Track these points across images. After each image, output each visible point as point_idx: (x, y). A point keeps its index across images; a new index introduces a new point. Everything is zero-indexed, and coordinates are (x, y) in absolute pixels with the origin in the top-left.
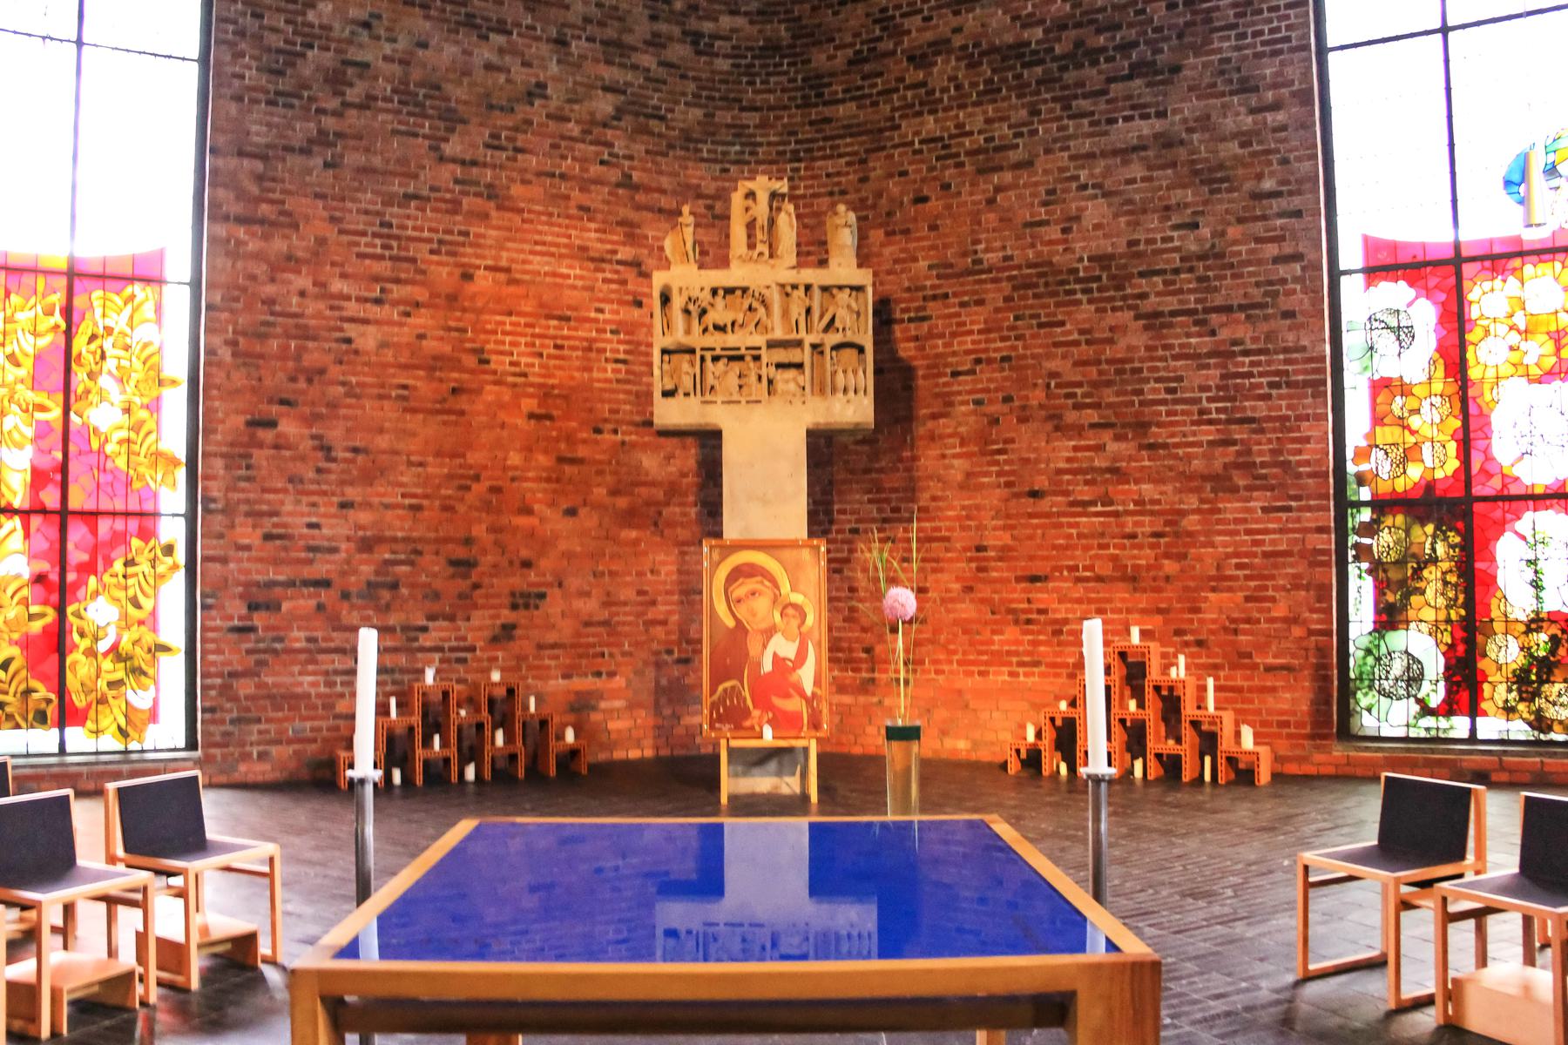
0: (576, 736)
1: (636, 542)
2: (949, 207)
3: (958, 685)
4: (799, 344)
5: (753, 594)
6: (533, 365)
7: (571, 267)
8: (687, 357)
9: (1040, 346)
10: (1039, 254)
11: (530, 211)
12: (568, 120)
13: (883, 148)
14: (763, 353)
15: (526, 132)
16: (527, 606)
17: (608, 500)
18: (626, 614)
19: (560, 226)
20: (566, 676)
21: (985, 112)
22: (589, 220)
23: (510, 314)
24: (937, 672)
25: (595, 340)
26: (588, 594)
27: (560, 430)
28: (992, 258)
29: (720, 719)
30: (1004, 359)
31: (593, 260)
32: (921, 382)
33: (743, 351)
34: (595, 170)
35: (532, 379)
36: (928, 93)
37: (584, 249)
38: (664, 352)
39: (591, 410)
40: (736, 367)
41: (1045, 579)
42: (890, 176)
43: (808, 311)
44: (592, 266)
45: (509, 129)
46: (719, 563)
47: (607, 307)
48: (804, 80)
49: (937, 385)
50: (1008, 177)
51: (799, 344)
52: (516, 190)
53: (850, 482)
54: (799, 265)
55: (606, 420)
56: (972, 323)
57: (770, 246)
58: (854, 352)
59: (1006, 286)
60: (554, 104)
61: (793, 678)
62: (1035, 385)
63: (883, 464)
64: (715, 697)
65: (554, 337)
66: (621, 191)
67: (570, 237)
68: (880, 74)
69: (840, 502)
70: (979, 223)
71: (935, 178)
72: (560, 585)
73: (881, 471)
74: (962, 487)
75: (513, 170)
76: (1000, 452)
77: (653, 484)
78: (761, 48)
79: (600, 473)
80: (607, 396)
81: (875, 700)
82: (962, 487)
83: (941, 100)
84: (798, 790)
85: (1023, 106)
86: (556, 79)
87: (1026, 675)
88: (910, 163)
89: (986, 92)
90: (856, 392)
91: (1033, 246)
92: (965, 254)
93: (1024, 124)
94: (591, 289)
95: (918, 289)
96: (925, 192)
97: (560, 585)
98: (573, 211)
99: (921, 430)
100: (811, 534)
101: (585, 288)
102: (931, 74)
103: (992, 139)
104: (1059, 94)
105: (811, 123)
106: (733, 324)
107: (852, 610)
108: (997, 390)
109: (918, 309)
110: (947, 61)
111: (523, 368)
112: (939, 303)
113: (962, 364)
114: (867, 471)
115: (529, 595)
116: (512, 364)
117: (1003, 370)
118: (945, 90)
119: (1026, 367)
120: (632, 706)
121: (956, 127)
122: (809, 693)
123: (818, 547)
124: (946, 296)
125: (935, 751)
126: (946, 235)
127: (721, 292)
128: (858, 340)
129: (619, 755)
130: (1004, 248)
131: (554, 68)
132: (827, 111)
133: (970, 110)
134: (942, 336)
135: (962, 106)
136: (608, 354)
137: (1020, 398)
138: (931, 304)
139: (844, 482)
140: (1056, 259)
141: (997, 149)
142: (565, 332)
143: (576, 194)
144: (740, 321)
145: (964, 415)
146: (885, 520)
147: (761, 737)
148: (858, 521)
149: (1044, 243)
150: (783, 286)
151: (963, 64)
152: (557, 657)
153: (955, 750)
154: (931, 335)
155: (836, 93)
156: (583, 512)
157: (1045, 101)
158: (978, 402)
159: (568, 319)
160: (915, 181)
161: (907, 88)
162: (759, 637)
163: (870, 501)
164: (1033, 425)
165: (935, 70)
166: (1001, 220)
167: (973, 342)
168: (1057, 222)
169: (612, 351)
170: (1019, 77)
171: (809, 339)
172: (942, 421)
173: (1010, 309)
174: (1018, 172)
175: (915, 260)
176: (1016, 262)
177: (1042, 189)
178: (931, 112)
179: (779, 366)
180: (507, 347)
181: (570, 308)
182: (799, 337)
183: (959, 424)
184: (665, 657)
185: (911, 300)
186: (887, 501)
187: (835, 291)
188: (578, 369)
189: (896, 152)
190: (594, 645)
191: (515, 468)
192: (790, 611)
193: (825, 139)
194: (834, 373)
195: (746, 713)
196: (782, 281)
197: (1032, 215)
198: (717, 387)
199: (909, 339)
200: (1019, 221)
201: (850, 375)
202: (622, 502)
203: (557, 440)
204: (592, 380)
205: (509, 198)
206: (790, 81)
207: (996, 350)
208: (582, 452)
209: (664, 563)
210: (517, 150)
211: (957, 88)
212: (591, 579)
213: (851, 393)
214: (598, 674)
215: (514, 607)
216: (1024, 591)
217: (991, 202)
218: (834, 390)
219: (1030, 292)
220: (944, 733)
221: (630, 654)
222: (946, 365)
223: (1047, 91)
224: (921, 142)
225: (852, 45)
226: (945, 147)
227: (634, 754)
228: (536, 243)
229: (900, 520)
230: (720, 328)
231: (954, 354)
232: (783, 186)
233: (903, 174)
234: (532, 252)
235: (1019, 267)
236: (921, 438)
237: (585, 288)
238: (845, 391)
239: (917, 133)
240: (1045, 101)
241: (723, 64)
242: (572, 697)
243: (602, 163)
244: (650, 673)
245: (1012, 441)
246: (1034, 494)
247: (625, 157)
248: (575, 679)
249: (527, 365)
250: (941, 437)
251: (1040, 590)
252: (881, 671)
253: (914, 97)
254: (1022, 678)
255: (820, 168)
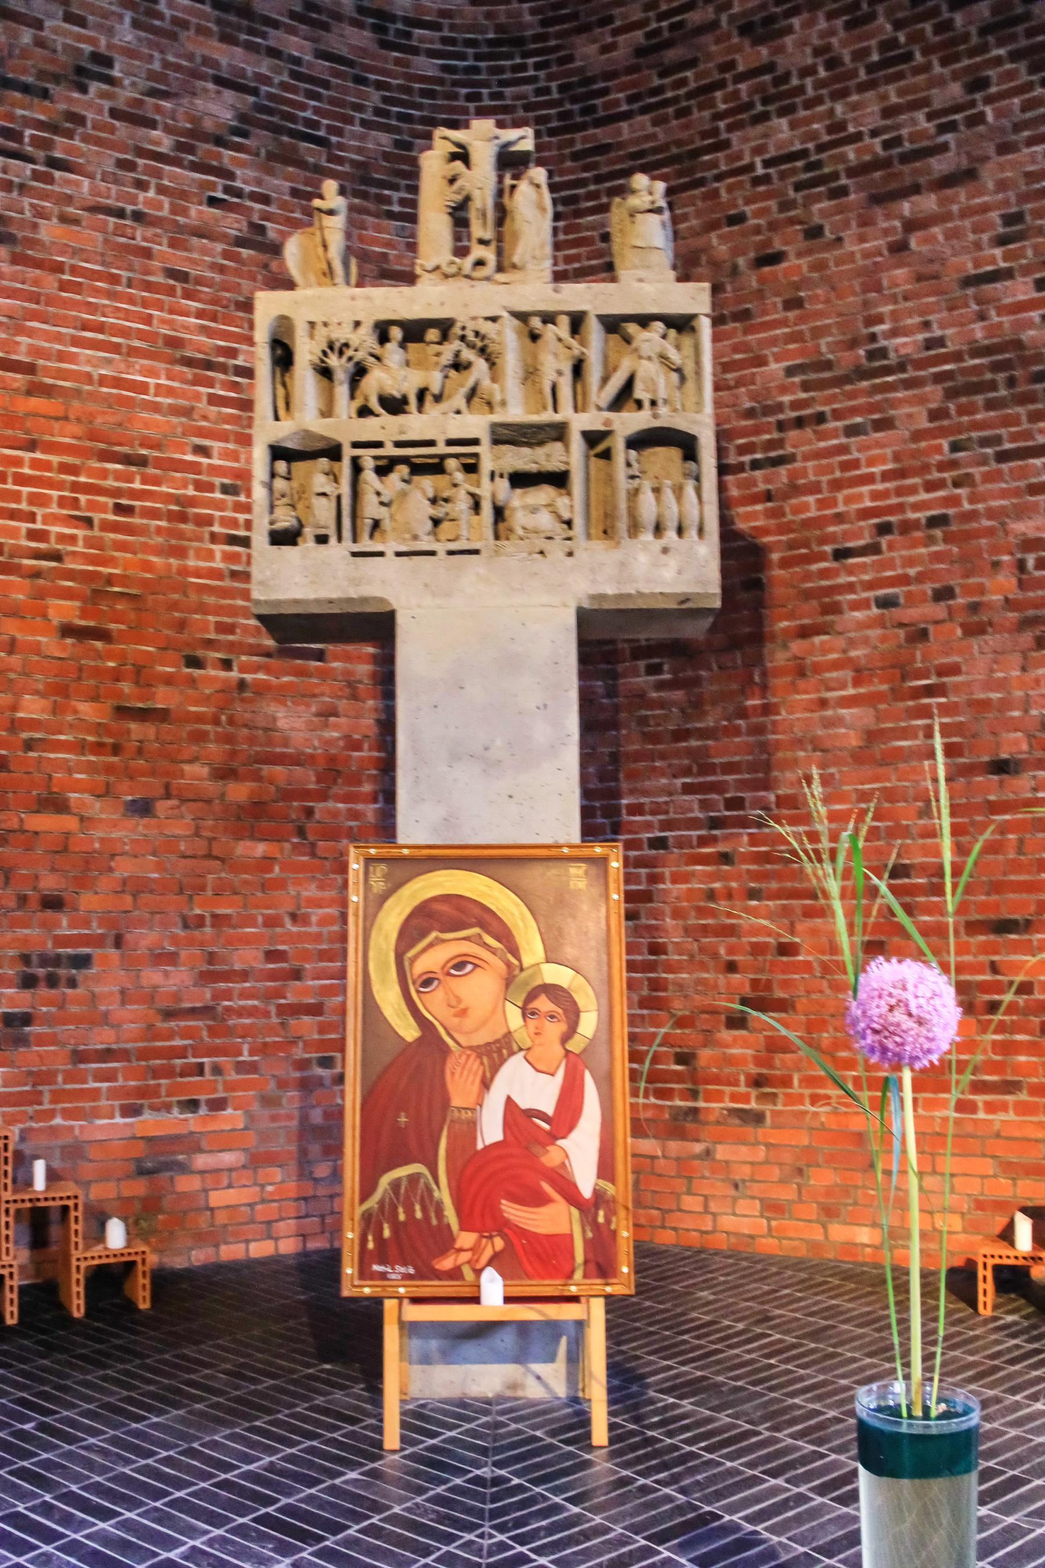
0: (130, 1235)
1: (266, 863)
2: (820, 266)
3: (856, 1125)
4: (559, 432)
5: (460, 966)
6: (72, 539)
7: (152, 373)
8: (324, 462)
9: (1004, 494)
10: (992, 330)
11: (74, 270)
12: (152, 124)
13: (701, 182)
14: (484, 450)
15: (69, 134)
16: (52, 981)
17: (211, 787)
18: (244, 995)
19: (131, 301)
20: (130, 1111)
21: (884, 97)
22: (188, 295)
23: (32, 446)
24: (815, 1099)
25: (192, 502)
26: (172, 958)
27: (122, 657)
28: (904, 345)
29: (383, 1253)
30: (934, 522)
31: (189, 362)
32: (777, 572)
33: (441, 449)
34: (198, 212)
35: (70, 565)
36: (778, 81)
37: (174, 343)
38: (278, 453)
39: (181, 625)
40: (428, 483)
41: (1027, 926)
42: (712, 226)
43: (578, 369)
44: (188, 372)
45: (40, 125)
46: (384, 898)
47: (216, 445)
48: (562, 89)
49: (808, 576)
50: (929, 202)
51: (559, 432)
52: (49, 231)
53: (651, 756)
54: (559, 277)
55: (209, 644)
56: (871, 462)
57: (499, 253)
58: (674, 454)
59: (934, 393)
60: (126, 94)
61: (551, 1157)
62: (996, 565)
63: (709, 722)
64: (372, 1202)
65: (116, 493)
66: (245, 252)
67: (148, 320)
68: (692, 63)
69: (632, 792)
70: (878, 288)
71: (792, 221)
72: (118, 942)
73: (704, 734)
74: (859, 757)
75: (45, 196)
76: (930, 691)
77: (296, 760)
78: (490, 43)
79: (200, 737)
80: (211, 600)
81: (698, 1148)
82: (859, 757)
83: (801, 90)
84: (562, 1391)
85: (955, 76)
86: (131, 53)
87: (990, 1108)
88: (748, 201)
89: (884, 64)
90: (680, 531)
91: (982, 317)
92: (853, 344)
93: (957, 109)
94: (187, 412)
95: (768, 411)
96: (778, 245)
97: (118, 942)
98: (159, 279)
99: (778, 657)
100: (589, 832)
101: (175, 411)
102: (780, 50)
103: (897, 141)
104: (1023, 43)
105: (576, 156)
106: (421, 395)
107: (656, 985)
108: (920, 578)
109: (771, 445)
110: (810, 23)
111: (54, 545)
112: (808, 432)
113: (857, 535)
114: (680, 735)
115: (57, 961)
116: (33, 535)
117: (931, 540)
118: (807, 71)
119: (977, 534)
120: (257, 1161)
121: (831, 129)
122: (587, 1192)
123: (604, 860)
124: (820, 418)
125: (814, 1246)
126: (819, 314)
127: (396, 333)
128: (681, 423)
129: (230, 1252)
130: (927, 325)
131: (126, 34)
132: (602, 135)
133: (854, 98)
134: (814, 488)
135: (840, 95)
136: (216, 528)
137: (968, 590)
138: (793, 434)
139: (638, 756)
140: (1029, 335)
141: (905, 158)
142: (137, 485)
143: (162, 248)
144: (435, 389)
145: (861, 625)
146: (716, 823)
147: (476, 1300)
148: (667, 825)
149: (1001, 310)
150: (522, 317)
151: (839, 22)
152: (109, 1076)
153: (850, 1246)
154: (795, 489)
155: (616, 103)
156: (162, 807)
157: (998, 61)
158: (885, 603)
159: (142, 462)
160: (757, 230)
161: (740, 78)
162: (474, 1064)
163: (688, 789)
164: (992, 640)
165: (789, 40)
166: (920, 278)
167: (875, 496)
168: (1026, 271)
169: (225, 522)
170: (943, 27)
171: (581, 422)
172: (817, 640)
173: (942, 432)
174: (949, 192)
175: (760, 361)
176: (951, 347)
177: (995, 216)
178: (783, 112)
179: (520, 480)
180: (24, 506)
181: (146, 443)
182: (558, 418)
183: (852, 643)
184: (320, 1071)
185: (757, 430)
186: (717, 788)
187: (632, 328)
188: (159, 551)
189: (722, 186)
190: (182, 1053)
191: (33, 724)
192: (543, 1004)
193: (598, 179)
194: (634, 494)
195: (445, 1242)
196: (524, 307)
197: (977, 264)
198: (386, 524)
199: (755, 499)
200: (950, 278)
201: (668, 495)
202: (239, 792)
203: (117, 676)
204: (184, 571)
205: (33, 243)
206: (539, 92)
207: (917, 507)
208: (163, 698)
209: (318, 904)
210: (54, 163)
211: (832, 64)
212: (179, 931)
213: (671, 535)
214: (192, 1105)
215: (28, 982)
216: (986, 949)
217: (899, 248)
218: (635, 528)
219: (979, 399)
220: (830, 1213)
221: (252, 1067)
222: (824, 540)
223: (1000, 44)
224: (767, 164)
225: (644, 23)
226: (811, 167)
227: (260, 1249)
228: (86, 326)
229: (744, 823)
230: (394, 405)
231: (839, 518)
232: (524, 139)
233: (738, 219)
234: (76, 342)
235: (957, 357)
236: (780, 672)
237: (175, 411)
238: (658, 529)
239: (758, 150)
240: (998, 61)
241: (426, 66)
242: (140, 1150)
243: (213, 202)
244: (291, 1099)
245: (954, 670)
246: (1001, 767)
247: (255, 197)
248: (147, 1116)
249: (62, 538)
250: (818, 668)
251: (1016, 948)
252: (709, 1097)
253: (752, 92)
254: (981, 1115)
255: (591, 227)
